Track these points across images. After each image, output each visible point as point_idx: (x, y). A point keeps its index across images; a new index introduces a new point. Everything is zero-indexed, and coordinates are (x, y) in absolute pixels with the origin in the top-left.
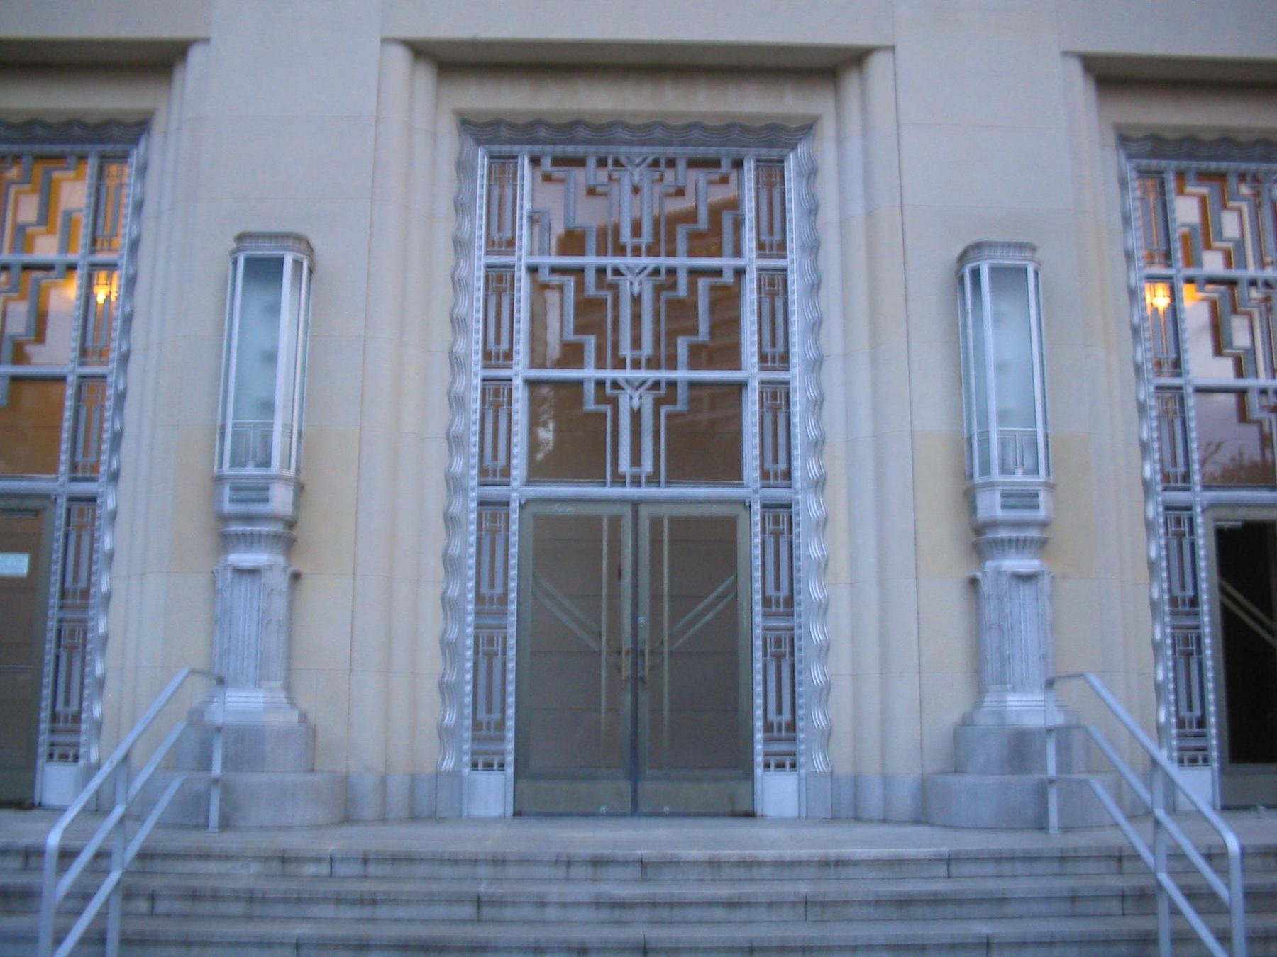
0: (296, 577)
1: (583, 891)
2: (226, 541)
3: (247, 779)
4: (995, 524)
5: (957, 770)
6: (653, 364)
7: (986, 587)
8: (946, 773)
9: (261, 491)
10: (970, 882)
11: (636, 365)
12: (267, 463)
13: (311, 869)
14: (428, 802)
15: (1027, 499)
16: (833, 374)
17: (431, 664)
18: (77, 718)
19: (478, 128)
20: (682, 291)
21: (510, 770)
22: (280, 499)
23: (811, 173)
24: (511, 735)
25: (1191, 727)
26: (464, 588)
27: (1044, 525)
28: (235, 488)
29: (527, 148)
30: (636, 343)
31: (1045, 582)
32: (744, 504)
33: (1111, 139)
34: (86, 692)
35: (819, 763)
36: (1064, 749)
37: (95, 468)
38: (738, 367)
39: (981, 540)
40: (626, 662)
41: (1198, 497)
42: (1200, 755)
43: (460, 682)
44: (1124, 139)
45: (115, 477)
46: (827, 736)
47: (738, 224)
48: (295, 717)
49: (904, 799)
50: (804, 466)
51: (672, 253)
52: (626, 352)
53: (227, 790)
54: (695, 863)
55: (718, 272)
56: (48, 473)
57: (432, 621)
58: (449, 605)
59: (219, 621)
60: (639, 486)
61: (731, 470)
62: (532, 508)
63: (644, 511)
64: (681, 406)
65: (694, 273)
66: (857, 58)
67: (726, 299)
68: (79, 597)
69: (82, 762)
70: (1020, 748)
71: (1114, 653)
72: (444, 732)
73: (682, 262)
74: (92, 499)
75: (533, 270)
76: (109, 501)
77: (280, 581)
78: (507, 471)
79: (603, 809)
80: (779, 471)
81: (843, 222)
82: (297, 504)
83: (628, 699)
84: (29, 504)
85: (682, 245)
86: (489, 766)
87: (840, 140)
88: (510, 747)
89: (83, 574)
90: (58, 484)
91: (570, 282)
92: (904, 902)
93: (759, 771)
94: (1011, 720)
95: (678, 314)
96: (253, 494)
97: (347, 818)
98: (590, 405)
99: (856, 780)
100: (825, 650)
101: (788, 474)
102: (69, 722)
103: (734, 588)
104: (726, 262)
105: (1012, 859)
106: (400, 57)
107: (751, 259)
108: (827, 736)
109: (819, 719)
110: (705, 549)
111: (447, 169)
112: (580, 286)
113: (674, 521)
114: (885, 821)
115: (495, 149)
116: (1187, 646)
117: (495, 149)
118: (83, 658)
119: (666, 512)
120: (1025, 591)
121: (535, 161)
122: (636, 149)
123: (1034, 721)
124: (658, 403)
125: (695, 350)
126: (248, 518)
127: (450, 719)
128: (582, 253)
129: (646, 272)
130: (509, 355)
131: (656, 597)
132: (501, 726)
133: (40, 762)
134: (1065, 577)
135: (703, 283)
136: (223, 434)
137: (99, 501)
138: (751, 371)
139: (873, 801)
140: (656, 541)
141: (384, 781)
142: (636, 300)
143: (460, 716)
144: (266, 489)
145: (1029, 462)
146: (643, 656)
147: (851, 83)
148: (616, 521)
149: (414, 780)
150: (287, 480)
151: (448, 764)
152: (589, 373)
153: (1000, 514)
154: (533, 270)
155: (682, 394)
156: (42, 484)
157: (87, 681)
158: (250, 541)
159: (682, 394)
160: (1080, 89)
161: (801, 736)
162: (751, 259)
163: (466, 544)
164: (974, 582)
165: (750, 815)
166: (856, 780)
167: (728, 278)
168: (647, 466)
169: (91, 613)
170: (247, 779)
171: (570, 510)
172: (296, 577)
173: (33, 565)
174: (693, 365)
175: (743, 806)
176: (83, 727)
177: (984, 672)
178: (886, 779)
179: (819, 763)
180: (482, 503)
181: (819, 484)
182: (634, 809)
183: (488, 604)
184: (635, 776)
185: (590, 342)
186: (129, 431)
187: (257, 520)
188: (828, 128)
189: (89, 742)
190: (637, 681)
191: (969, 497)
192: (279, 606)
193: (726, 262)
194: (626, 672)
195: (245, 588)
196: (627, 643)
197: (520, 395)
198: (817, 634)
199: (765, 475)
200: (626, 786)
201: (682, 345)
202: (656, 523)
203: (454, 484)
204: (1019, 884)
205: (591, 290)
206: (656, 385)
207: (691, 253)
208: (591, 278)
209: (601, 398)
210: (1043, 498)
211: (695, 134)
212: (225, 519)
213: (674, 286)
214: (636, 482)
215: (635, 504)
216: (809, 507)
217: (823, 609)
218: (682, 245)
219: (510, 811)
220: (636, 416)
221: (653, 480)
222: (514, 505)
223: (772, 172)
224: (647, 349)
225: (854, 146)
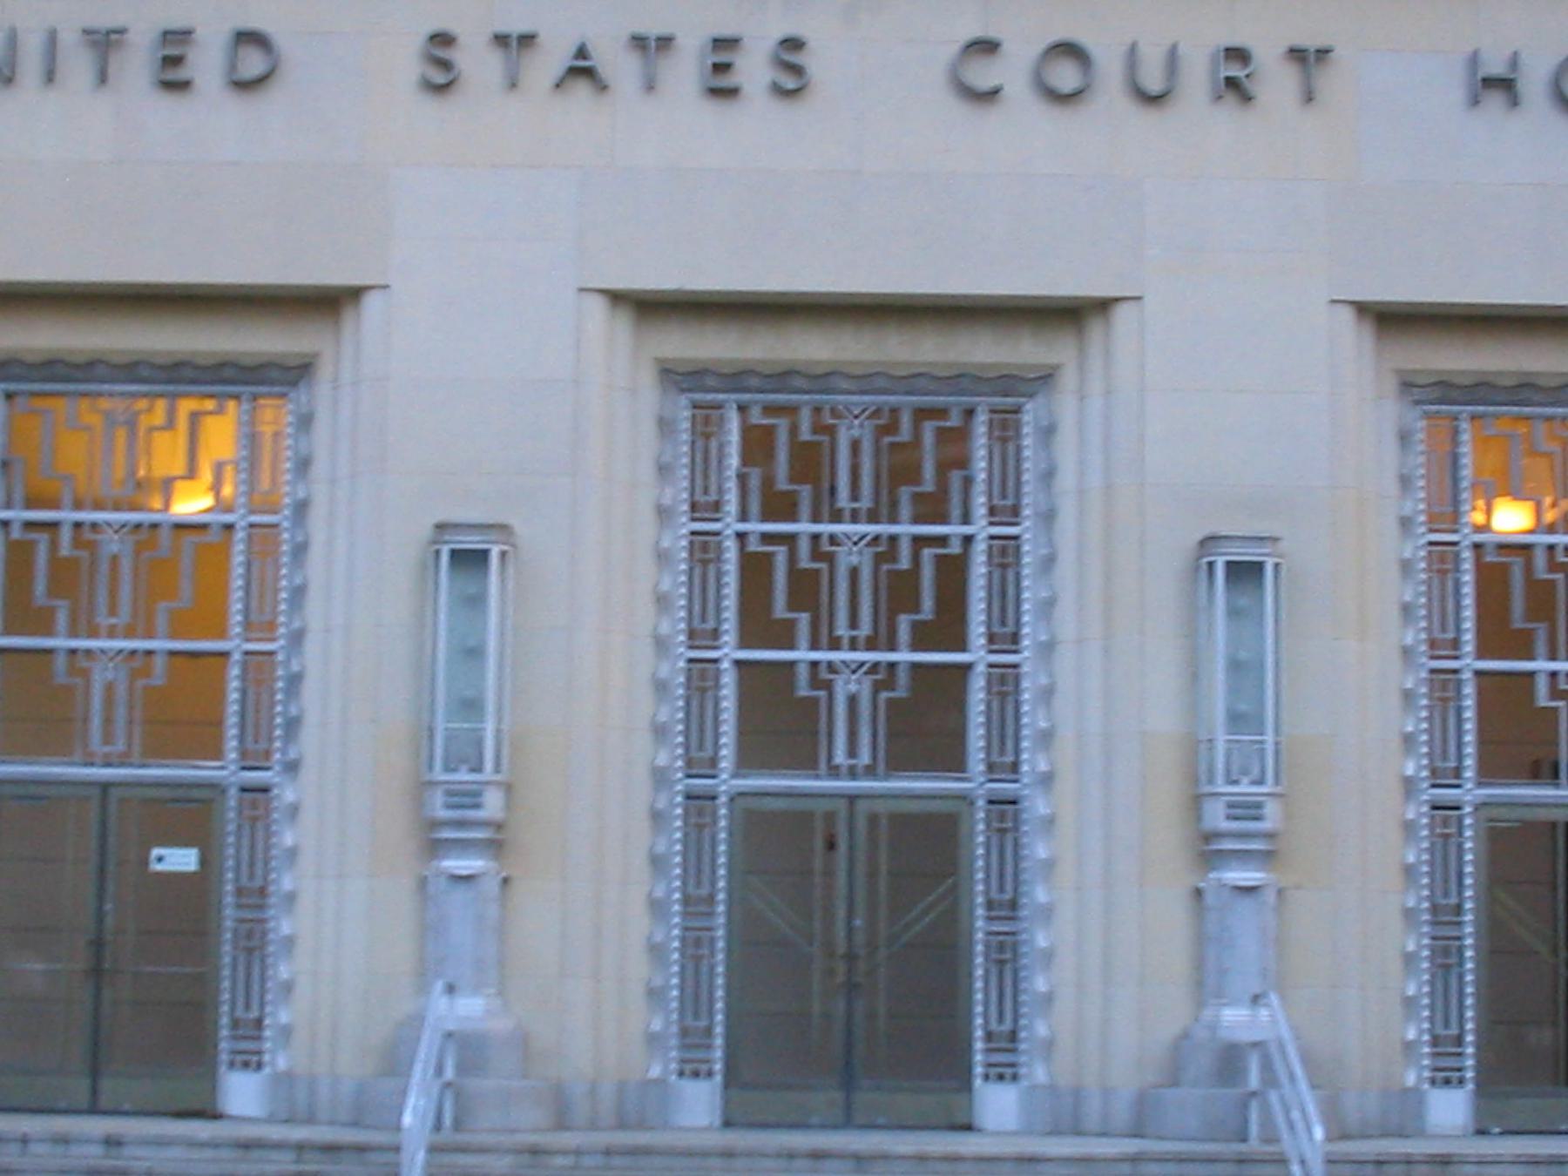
0: (506, 881)
2: (435, 848)
3: (473, 1084)
5: (1175, 1083)
6: (871, 645)
7: (1210, 899)
8: (1161, 1086)
11: (853, 646)
12: (478, 769)
15: (1247, 810)
16: (1065, 658)
17: (639, 968)
18: (259, 1023)
19: (676, 377)
20: (904, 563)
21: (718, 1078)
22: (493, 805)
23: (1048, 432)
24: (719, 1041)
26: (671, 892)
27: (1269, 836)
28: (449, 793)
29: (734, 396)
30: (854, 623)
31: (1270, 897)
32: (965, 799)
33: (1391, 384)
34: (269, 997)
35: (1040, 1074)
36: (1267, 1066)
37: (267, 754)
38: (962, 646)
39: (1208, 850)
40: (841, 968)
42: (1009, 1071)
43: (667, 987)
44: (1407, 385)
45: (292, 767)
46: (1049, 1045)
47: (968, 482)
49: (1121, 1114)
50: (1033, 762)
51: (893, 520)
52: (842, 631)
53: (459, 1097)
54: (903, 1158)
55: (942, 540)
56: (212, 759)
57: (640, 924)
59: (429, 930)
60: (851, 776)
61: (955, 762)
62: (740, 802)
63: (862, 807)
64: (901, 693)
65: (919, 541)
66: (355, 294)
67: (953, 572)
68: (256, 896)
69: (267, 1070)
71: (1354, 964)
72: (652, 1039)
73: (905, 529)
74: (265, 790)
75: (741, 536)
76: (287, 794)
77: (491, 886)
78: (714, 762)
79: (815, 1120)
80: (1005, 766)
81: (1081, 492)
83: (840, 1005)
84: (196, 793)
85: (905, 510)
86: (696, 1074)
88: (718, 1053)
89: (259, 872)
90: (225, 770)
91: (781, 552)
93: (978, 1082)
94: (1224, 1034)
95: (899, 592)
96: (466, 800)
97: (561, 1125)
98: (803, 691)
99: (1077, 1093)
100: (1048, 956)
101: (1015, 767)
103: (955, 886)
104: (953, 529)
105: (1193, 1160)
106: (597, 308)
107: (981, 527)
108: (1049, 1045)
109: (1042, 1029)
110: (929, 842)
111: (648, 428)
112: (792, 558)
114: (1104, 1134)
115: (698, 396)
116: (1445, 957)
117: (698, 396)
118: (263, 961)
119: (881, 807)
121: (742, 409)
122: (855, 398)
123: (1245, 1036)
124: (877, 687)
125: (916, 627)
126: (461, 824)
128: (792, 517)
129: (865, 669)
130: (716, 633)
131: (872, 875)
132: (709, 1032)
133: (223, 1069)
134: (1298, 887)
135: (928, 553)
136: (431, 737)
137: (276, 791)
140: (873, 841)
141: (593, 1090)
143: (667, 1023)
144: (478, 794)
145: (1256, 771)
147: (1095, 329)
148: (830, 817)
149: (622, 1087)
150: (498, 784)
151: (655, 1071)
152: (802, 654)
153: (1226, 825)
154: (741, 536)
155: (903, 677)
156: (205, 771)
157: (269, 984)
158: (464, 846)
159: (903, 677)
160: (1350, 334)
161: (1023, 1046)
162: (981, 527)
163: (673, 842)
165: (968, 1128)
167: (955, 549)
168: (865, 758)
169: (272, 912)
170: (473, 1084)
171: (781, 804)
173: (204, 861)
174: (916, 646)
175: (960, 1119)
176: (267, 1033)
177: (1206, 983)
178: (1107, 1093)
180: (689, 797)
181: (1047, 780)
184: (848, 1084)
187: (459, 818)
188: (1068, 379)
189: (273, 1052)
190: (851, 988)
191: (1196, 802)
192: (493, 911)
193: (953, 529)
194: (840, 978)
195: (460, 894)
196: (841, 949)
197: (729, 680)
198: (1041, 941)
199: (991, 767)
200: (838, 1096)
201: (904, 623)
202: (873, 819)
203: (660, 777)
205: (805, 563)
207: (917, 520)
208: (804, 547)
209: (816, 682)
210: (1271, 809)
212: (436, 824)
213: (146, 672)
214: (853, 773)
215: (852, 798)
216: (1038, 805)
217: (1047, 912)
218: (905, 510)
219: (718, 1122)
220: (853, 701)
221: (870, 771)
222: (723, 799)
223: (1006, 427)
224: (865, 630)
225: (1095, 404)
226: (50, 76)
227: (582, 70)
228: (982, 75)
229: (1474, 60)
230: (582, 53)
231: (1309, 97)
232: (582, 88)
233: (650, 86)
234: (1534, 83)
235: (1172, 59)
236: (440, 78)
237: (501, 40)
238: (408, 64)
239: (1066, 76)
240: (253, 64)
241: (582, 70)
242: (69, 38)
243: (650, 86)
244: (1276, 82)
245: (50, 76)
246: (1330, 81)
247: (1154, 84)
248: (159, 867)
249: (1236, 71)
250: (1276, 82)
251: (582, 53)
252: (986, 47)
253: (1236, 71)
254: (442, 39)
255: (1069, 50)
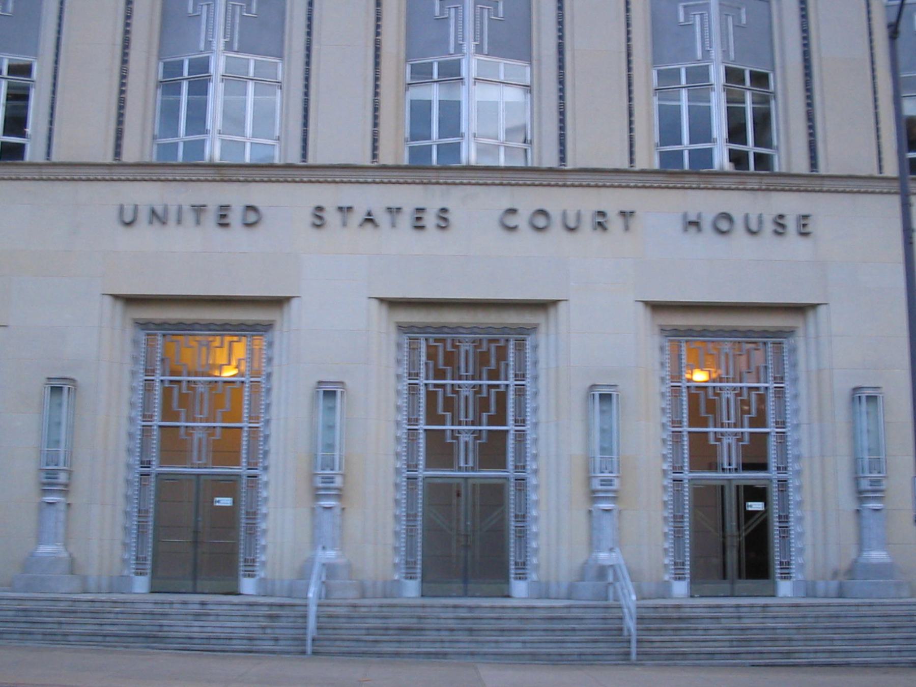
1: (451, 615)
2: (318, 497)
4: (598, 491)
6: (473, 424)
7: (594, 514)
9: (330, 479)
10: (576, 613)
13: (363, 609)
14: (391, 589)
15: (608, 482)
16: (542, 429)
19: (402, 328)
25: (678, 565)
31: (615, 513)
33: (657, 329)
37: (256, 464)
38: (505, 425)
39: (594, 496)
40: (462, 539)
41: (687, 475)
44: (663, 330)
45: (266, 468)
46: (537, 567)
48: (64, 555)
49: (563, 591)
55: (497, 386)
58: (397, 518)
59: (315, 527)
60: (465, 470)
61: (503, 465)
63: (470, 481)
65: (490, 386)
67: (502, 398)
68: (252, 515)
70: (602, 572)
73: (485, 382)
76: (264, 478)
80: (521, 467)
82: (344, 483)
84: (232, 478)
85: (485, 375)
87: (547, 335)
90: (242, 470)
92: (551, 619)
93: (512, 580)
94: (600, 562)
95: (483, 404)
97: (363, 597)
99: (548, 583)
102: (251, 562)
103: (503, 512)
107: (512, 382)
109: (535, 561)
110: (493, 497)
112: (445, 392)
113: (481, 485)
116: (678, 534)
119: (478, 482)
120: (607, 515)
125: (489, 417)
127: (397, 560)
138: (511, 427)
139: (553, 592)
142: (467, 398)
144: (332, 478)
146: (468, 532)
147: (552, 311)
151: (396, 577)
159: (484, 435)
163: (402, 496)
164: (590, 512)
166: (548, 583)
167: (502, 389)
168: (471, 464)
171: (439, 481)
172: (343, 509)
175: (506, 593)
177: (593, 544)
179: (800, 577)
181: (536, 472)
182: (465, 595)
183: (411, 517)
184: (466, 581)
185: (449, 414)
186: (273, 451)
187: (326, 487)
188: (542, 329)
191: (589, 479)
195: (326, 515)
204: (590, 614)
206: (474, 386)
208: (449, 389)
209: (453, 437)
211: (259, 328)
214: (467, 470)
215: (466, 478)
218: (485, 375)
221: (473, 469)
222: (420, 479)
223: (520, 346)
224: (471, 418)
226: (179, 221)
227: (369, 220)
228: (511, 221)
229: (685, 215)
230: (369, 214)
231: (627, 228)
232: (369, 226)
233: (393, 225)
234: (707, 223)
235: (579, 216)
236: (318, 222)
237: (340, 209)
238: (307, 217)
239: (541, 222)
240: (252, 217)
241: (369, 220)
242: (186, 208)
243: (393, 225)
244: (615, 223)
245: (179, 221)
246: (634, 223)
247: (754, 227)
248: (750, 509)
249: (601, 220)
250: (615, 223)
251: (369, 214)
252: (512, 211)
253: (601, 220)
254: (320, 209)
255: (542, 212)
